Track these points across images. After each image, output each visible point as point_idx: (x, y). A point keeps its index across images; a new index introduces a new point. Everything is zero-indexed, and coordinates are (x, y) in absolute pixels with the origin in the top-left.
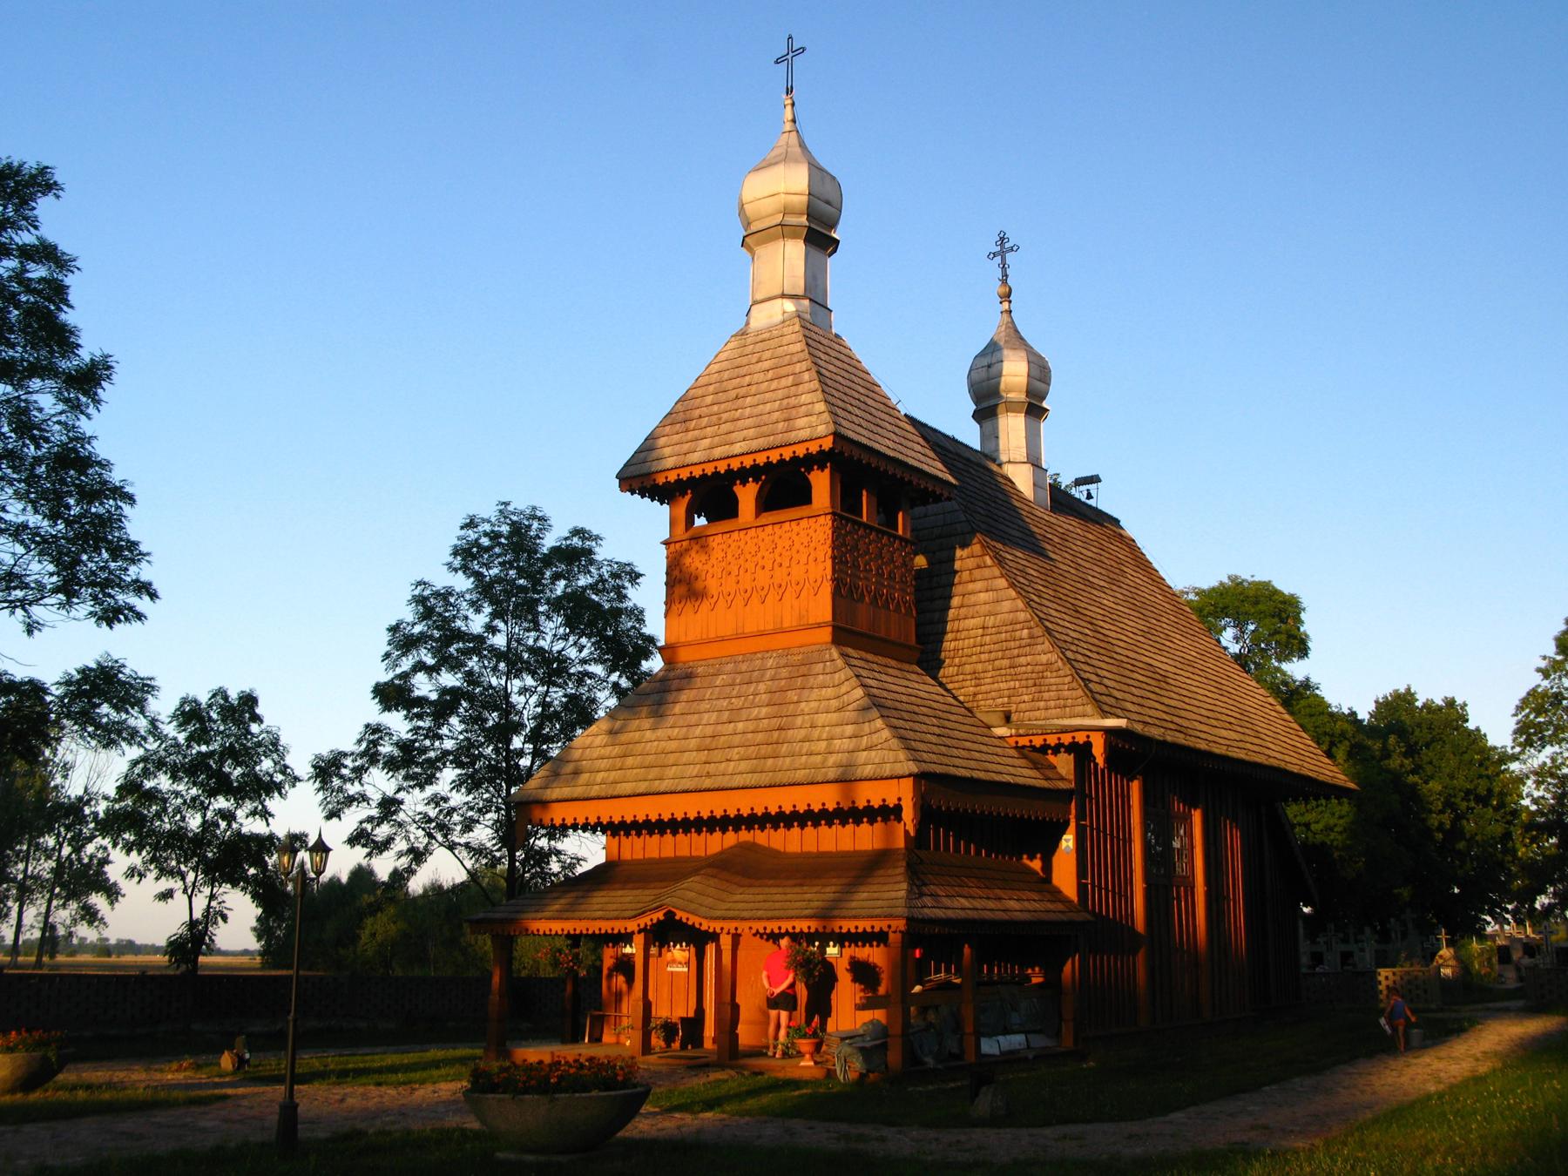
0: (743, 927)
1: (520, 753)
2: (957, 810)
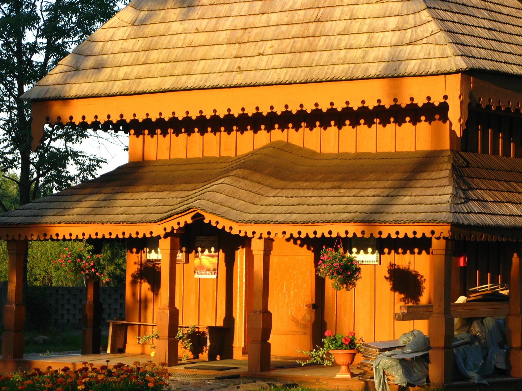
0: (276, 231)
1: (33, 48)
2: (508, 109)
